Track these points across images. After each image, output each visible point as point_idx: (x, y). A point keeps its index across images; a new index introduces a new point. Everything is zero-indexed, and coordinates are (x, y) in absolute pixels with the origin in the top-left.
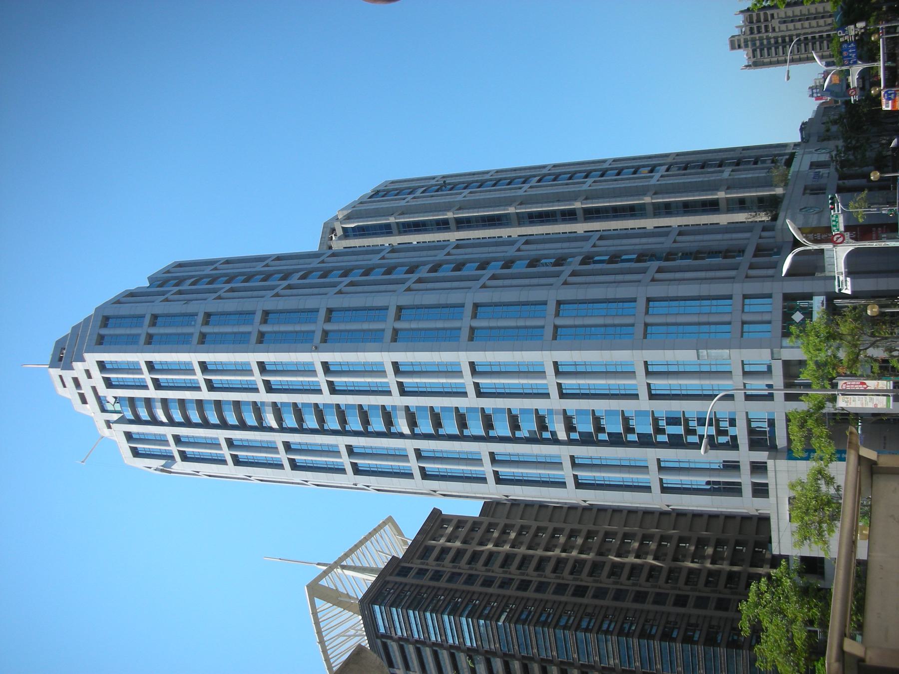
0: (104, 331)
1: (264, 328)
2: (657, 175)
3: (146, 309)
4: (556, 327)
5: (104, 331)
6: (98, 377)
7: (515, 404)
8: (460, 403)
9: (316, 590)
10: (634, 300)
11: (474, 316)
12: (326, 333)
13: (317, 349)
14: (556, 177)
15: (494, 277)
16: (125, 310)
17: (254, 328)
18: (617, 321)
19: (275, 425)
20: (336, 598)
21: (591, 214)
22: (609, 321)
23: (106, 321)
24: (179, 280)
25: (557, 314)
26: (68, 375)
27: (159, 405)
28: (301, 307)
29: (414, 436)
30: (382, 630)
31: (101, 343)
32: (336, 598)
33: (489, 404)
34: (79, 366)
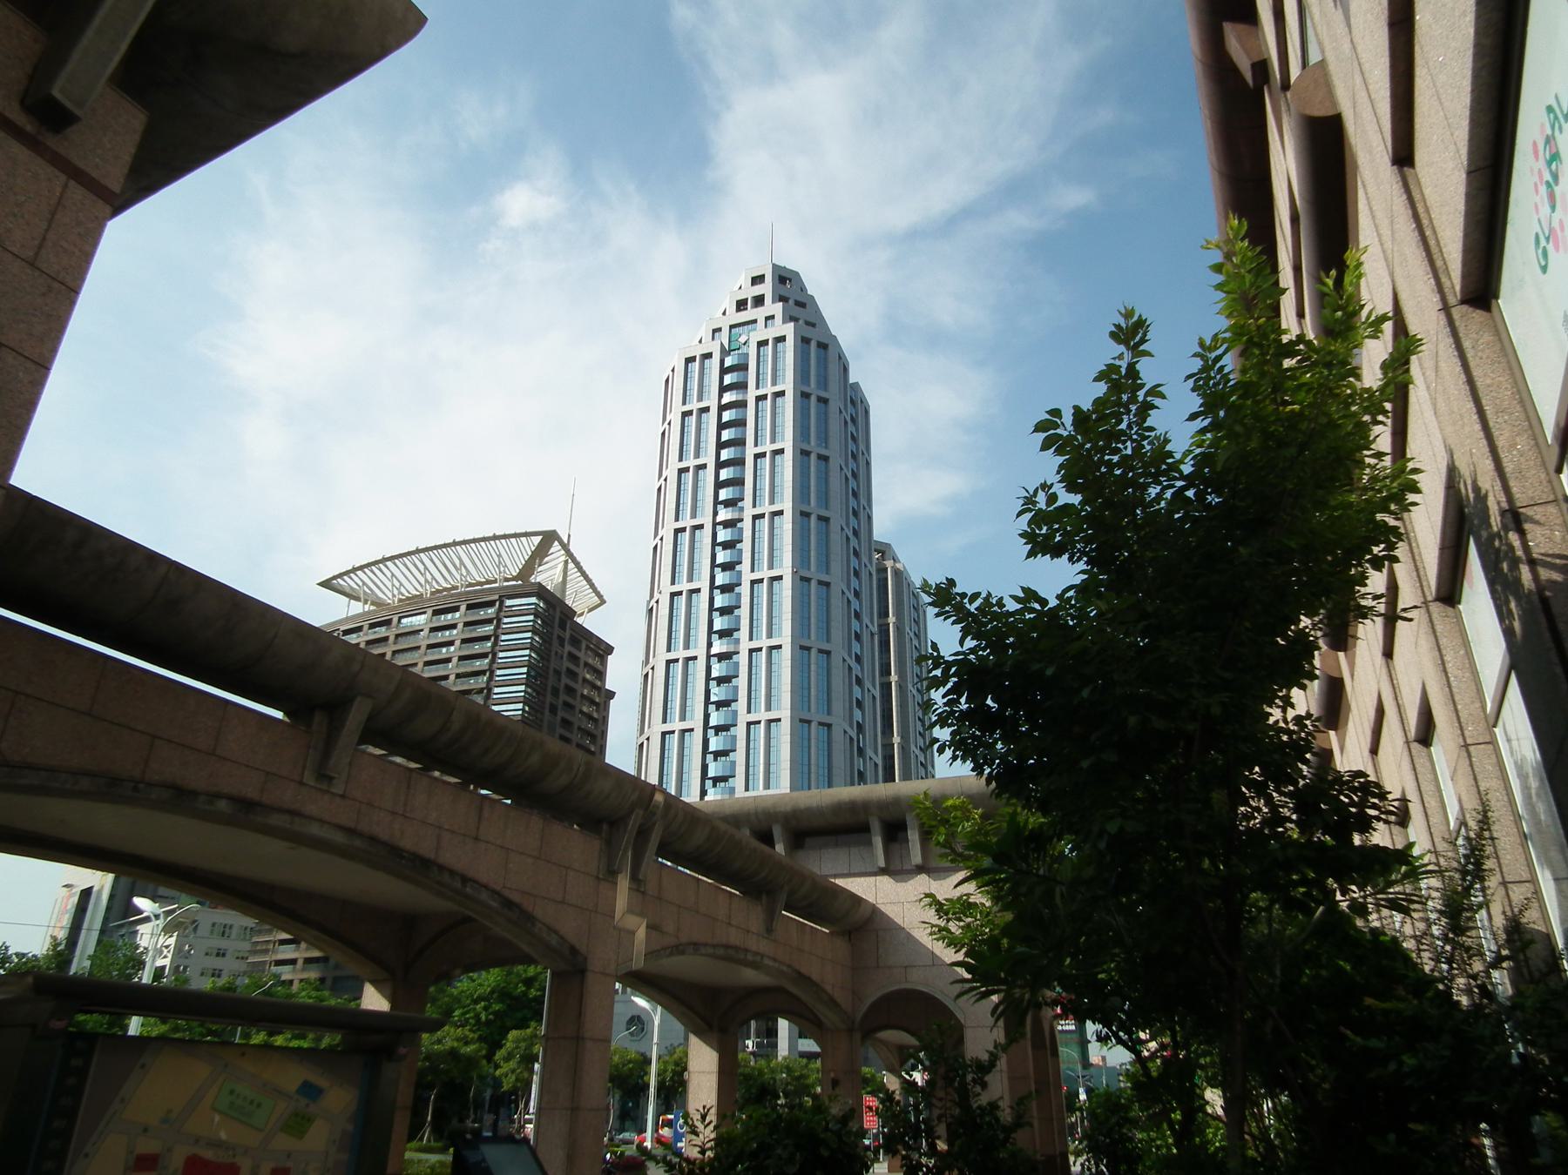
0: (813, 344)
1: (813, 399)
2: (918, 752)
3: (833, 394)
4: (809, 722)
5: (813, 344)
6: (770, 334)
7: (739, 756)
8: (741, 705)
9: (549, 537)
10: (829, 713)
11: (820, 651)
12: (808, 580)
13: (794, 573)
14: (917, 623)
15: (850, 668)
16: (834, 370)
17: (813, 445)
18: (813, 776)
19: (724, 401)
20: (540, 553)
21: (884, 613)
22: (813, 768)
23: (823, 346)
24: (856, 410)
25: (820, 724)
26: (766, 289)
27: (740, 397)
28: (832, 557)
29: (715, 524)
30: (508, 602)
31: (803, 341)
32: (540, 553)
33: (745, 589)
34: (777, 309)
